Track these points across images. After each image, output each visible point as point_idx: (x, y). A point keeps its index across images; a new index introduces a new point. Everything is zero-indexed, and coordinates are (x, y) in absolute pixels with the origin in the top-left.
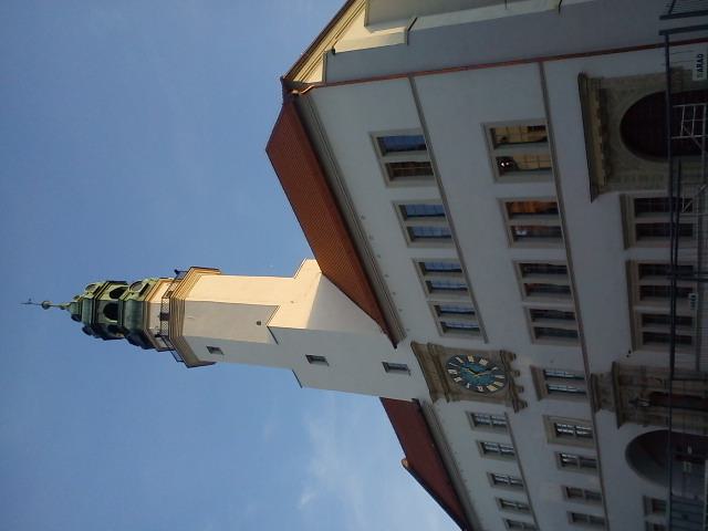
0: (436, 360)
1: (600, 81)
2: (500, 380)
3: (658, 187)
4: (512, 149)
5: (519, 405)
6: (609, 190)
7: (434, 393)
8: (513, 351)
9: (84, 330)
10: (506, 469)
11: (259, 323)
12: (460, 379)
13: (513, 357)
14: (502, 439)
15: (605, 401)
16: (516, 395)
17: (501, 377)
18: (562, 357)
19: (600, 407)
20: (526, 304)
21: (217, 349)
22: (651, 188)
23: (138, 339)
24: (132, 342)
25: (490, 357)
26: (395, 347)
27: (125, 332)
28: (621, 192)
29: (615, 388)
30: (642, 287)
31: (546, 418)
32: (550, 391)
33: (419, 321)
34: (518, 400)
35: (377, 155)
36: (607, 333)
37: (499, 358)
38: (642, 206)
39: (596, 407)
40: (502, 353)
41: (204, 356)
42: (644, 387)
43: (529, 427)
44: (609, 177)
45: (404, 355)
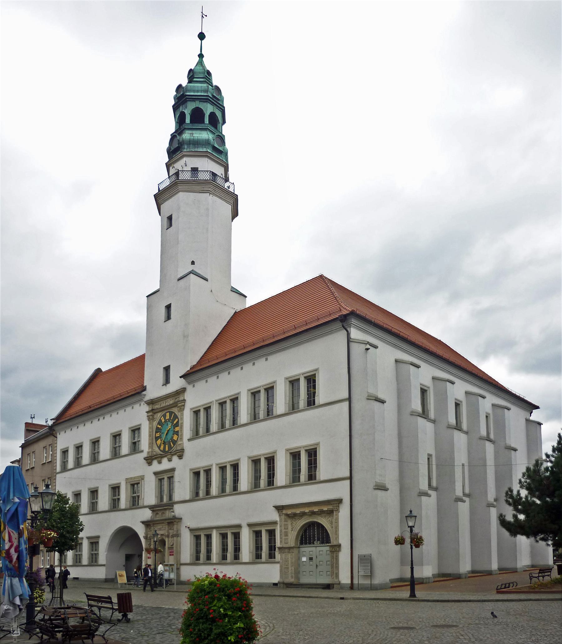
0: (175, 405)
1: (338, 510)
2: (165, 448)
3: (281, 542)
4: (306, 463)
5: (149, 460)
6: (280, 516)
7: (151, 402)
8: (184, 457)
9: (180, 86)
10: (105, 451)
11: (193, 263)
12: (163, 421)
13: (180, 457)
14: (125, 448)
15: (157, 514)
16: (156, 458)
17: (167, 449)
18: (182, 488)
19: (153, 511)
20: (214, 466)
21: (171, 225)
22: (281, 538)
23: (176, 145)
24: (173, 137)
25: (179, 443)
26: (181, 377)
27: (179, 131)
28: (279, 523)
29: (166, 520)
30: (227, 534)
31: (142, 478)
32: (161, 480)
33: (197, 396)
34: (153, 460)
35: (193, 408)
36: (194, 515)
37: (179, 448)
38: (272, 533)
39: (152, 508)
40: (182, 450)
41: (167, 206)
42: (168, 536)
43: (134, 466)
44: (287, 515)
45: (176, 383)
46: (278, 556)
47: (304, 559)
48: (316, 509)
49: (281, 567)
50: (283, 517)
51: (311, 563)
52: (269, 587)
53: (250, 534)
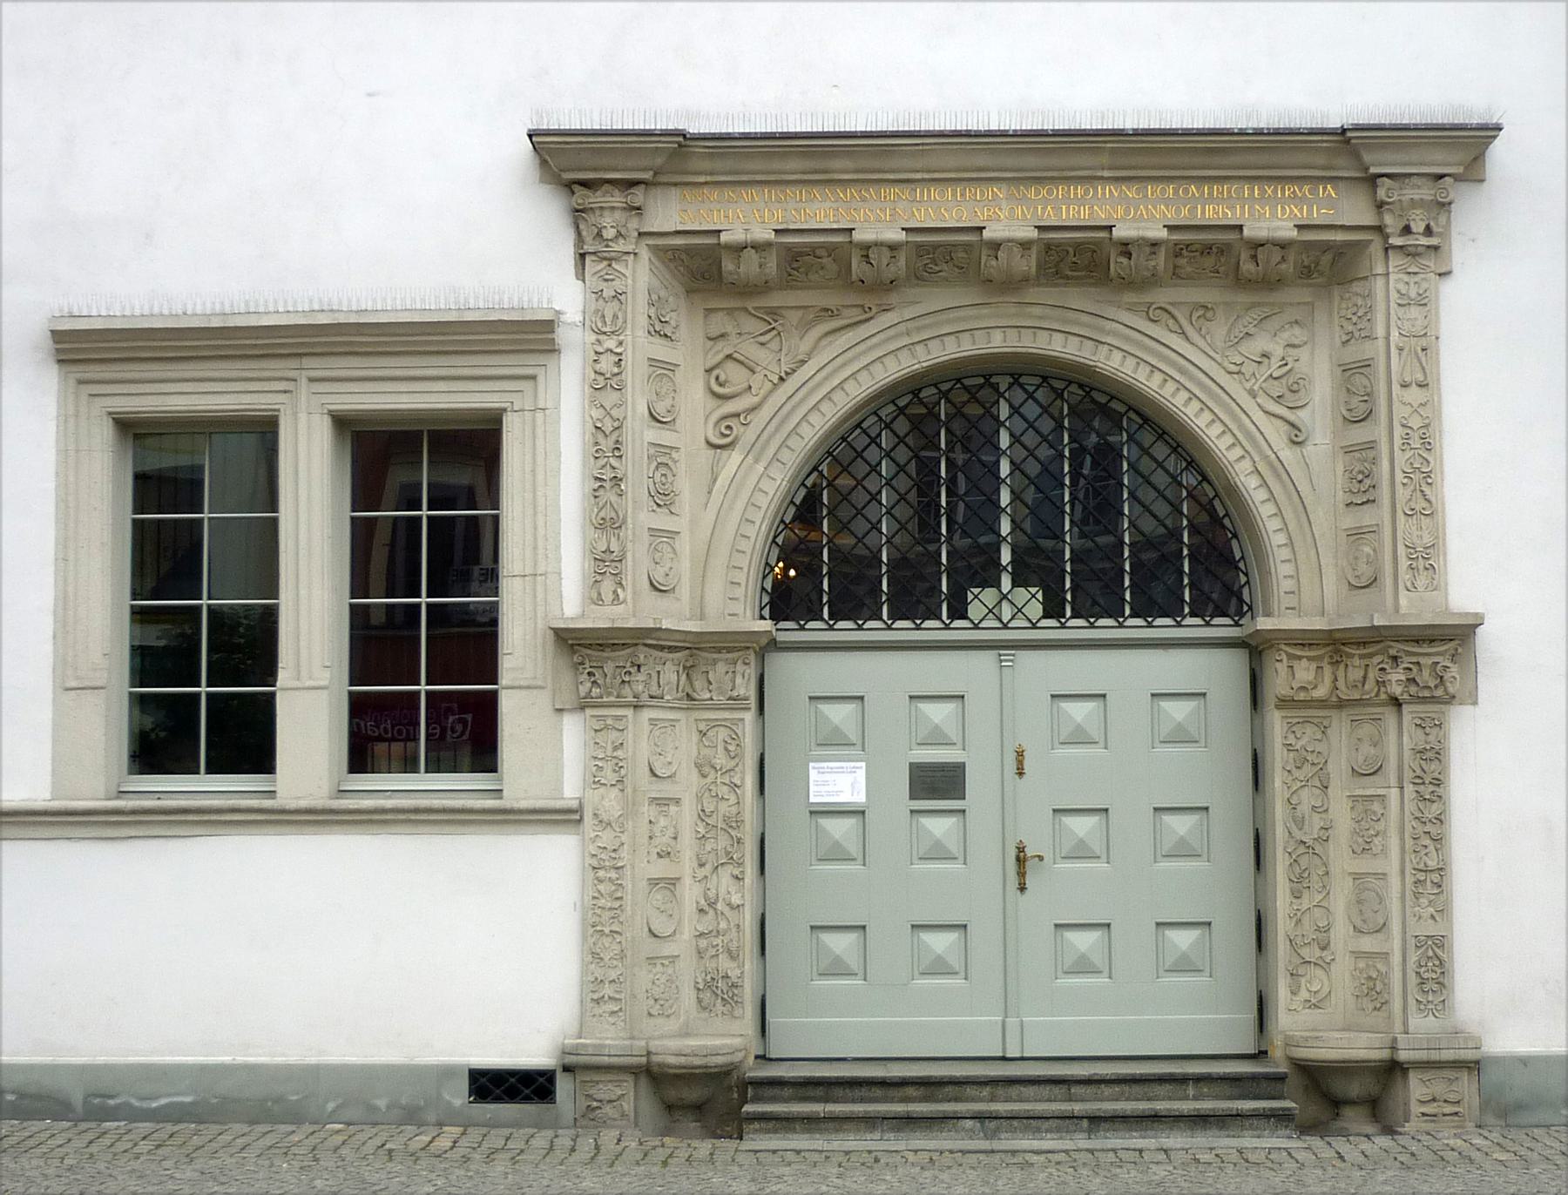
1: (1427, 250)
30: (264, 431)
46: (543, 737)
47: (838, 782)
48: (1141, 214)
49: (603, 872)
50: (639, 275)
51: (940, 827)
52: (411, 1116)
53: (70, 456)
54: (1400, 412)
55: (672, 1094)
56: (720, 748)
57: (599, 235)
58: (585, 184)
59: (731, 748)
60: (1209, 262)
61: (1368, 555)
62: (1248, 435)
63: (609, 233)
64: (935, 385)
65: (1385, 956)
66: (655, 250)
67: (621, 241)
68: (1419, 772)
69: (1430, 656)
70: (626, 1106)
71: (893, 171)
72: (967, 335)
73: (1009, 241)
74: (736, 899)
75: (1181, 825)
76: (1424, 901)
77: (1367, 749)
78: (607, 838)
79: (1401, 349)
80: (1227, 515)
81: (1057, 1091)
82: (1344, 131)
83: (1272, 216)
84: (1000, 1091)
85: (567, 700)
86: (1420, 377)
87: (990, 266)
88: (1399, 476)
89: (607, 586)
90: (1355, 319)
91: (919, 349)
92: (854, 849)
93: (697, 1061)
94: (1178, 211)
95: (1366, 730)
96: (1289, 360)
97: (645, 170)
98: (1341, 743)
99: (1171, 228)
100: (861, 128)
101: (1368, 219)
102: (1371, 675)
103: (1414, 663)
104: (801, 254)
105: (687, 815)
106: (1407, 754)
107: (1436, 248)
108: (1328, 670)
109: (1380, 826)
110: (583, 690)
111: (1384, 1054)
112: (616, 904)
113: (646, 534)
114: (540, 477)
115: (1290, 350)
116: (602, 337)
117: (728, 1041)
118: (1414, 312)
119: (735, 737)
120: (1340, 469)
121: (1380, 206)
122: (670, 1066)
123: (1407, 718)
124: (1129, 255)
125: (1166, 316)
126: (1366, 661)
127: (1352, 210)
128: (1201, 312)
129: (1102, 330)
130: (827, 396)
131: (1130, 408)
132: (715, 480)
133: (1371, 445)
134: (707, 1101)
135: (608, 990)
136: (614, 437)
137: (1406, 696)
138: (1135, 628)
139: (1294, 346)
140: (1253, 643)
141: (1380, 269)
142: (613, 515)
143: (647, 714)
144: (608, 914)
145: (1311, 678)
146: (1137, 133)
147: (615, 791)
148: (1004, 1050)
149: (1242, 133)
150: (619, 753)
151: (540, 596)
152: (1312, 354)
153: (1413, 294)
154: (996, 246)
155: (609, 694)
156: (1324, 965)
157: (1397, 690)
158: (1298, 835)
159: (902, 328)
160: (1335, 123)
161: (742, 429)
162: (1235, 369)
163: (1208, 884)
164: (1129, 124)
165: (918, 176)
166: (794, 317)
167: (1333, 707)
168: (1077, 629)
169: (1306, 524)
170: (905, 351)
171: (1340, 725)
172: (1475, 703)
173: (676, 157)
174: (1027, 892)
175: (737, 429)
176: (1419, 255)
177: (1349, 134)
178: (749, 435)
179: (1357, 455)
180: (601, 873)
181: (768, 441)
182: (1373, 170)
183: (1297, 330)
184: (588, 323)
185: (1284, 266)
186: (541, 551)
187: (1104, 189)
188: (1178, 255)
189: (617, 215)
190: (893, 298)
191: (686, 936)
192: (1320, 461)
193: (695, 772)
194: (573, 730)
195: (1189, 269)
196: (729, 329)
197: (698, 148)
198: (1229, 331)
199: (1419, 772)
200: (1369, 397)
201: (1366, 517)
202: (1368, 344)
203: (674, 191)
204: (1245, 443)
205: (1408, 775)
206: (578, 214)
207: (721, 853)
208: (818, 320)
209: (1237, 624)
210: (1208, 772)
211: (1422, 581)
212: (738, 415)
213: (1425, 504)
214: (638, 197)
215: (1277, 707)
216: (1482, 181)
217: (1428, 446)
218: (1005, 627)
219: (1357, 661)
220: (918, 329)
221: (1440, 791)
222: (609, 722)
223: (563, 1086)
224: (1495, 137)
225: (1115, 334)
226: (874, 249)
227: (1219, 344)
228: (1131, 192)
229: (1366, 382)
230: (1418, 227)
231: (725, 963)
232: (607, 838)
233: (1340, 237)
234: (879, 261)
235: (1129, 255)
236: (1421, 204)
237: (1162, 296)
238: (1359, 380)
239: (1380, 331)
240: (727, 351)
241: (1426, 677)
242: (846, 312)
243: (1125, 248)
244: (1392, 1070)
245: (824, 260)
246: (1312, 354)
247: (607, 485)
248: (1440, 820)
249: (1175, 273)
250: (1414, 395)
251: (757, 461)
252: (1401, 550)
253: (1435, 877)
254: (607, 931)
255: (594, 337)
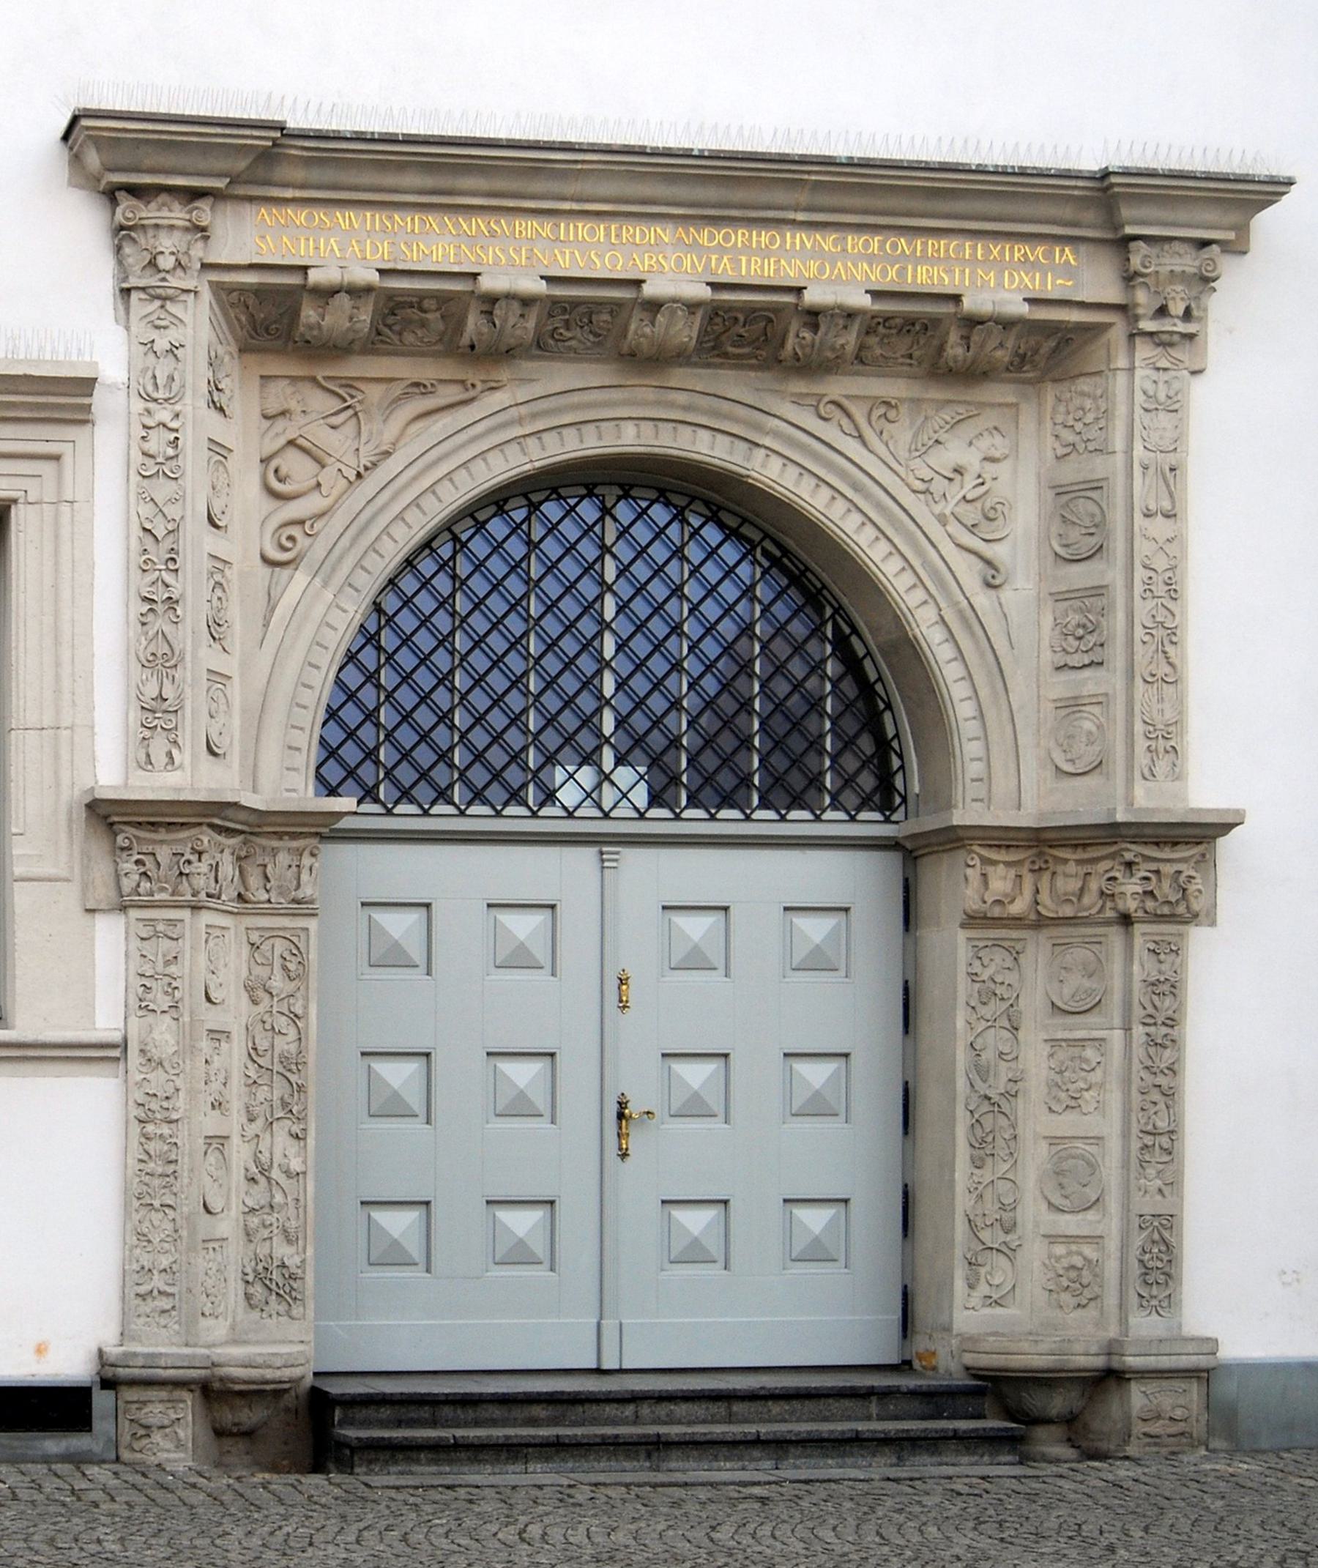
1: (1174, 334)
48: (838, 270)
50: (198, 323)
54: (1143, 548)
55: (227, 1417)
56: (277, 963)
57: (152, 264)
58: (135, 191)
59: (292, 966)
60: (902, 345)
61: (1090, 733)
62: (935, 574)
63: (166, 262)
64: (525, 496)
65: (1096, 1240)
66: (217, 288)
67: (179, 272)
68: (1150, 1010)
69: (1176, 860)
70: (181, 1434)
71: (533, 197)
72: (591, 427)
73: (674, 300)
74: (296, 1165)
75: (816, 1074)
76: (1151, 1172)
77: (1076, 981)
78: (158, 1081)
79: (1146, 468)
80: (880, 679)
81: (719, 1409)
82: (1106, 174)
83: (999, 280)
84: (645, 1410)
85: (103, 892)
86: (1166, 505)
87: (639, 330)
88: (1139, 633)
89: (159, 747)
90: (1079, 427)
91: (531, 442)
92: (540, 1100)
93: (269, 1374)
94: (884, 273)
95: (1080, 954)
96: (987, 476)
97: (219, 175)
98: (1037, 974)
99: (876, 295)
100: (503, 135)
101: (1112, 294)
102: (1094, 885)
103: (1143, 868)
104: (401, 305)
105: (235, 1053)
106: (1137, 986)
107: (1190, 337)
108: (1028, 880)
109: (1096, 1077)
110: (127, 884)
111: (1099, 1362)
112: (171, 1168)
113: (205, 676)
114: (66, 594)
115: (987, 465)
116: (151, 405)
117: (284, 1349)
118: (1164, 419)
119: (297, 951)
120: (1048, 621)
121: (1129, 278)
122: (234, 1381)
123: (1138, 941)
124: (815, 327)
125: (837, 414)
126: (1088, 868)
127: (1093, 280)
128: (882, 410)
129: (759, 428)
130: (415, 503)
131: (767, 536)
132: (273, 610)
133: (1098, 591)
134: (318, 1428)
135: (158, 1282)
136: (167, 544)
137: (1140, 914)
138: (765, 821)
139: (993, 460)
140: (909, 845)
141: (1122, 362)
142: (166, 649)
143: (206, 918)
144: (156, 1182)
145: (1008, 890)
146: (851, 163)
147: (167, 1018)
148: (599, 1359)
149: (981, 170)
150: (173, 969)
151: (65, 756)
152: (1015, 471)
153: (1162, 397)
154: (654, 306)
155: (163, 889)
156: (1009, 1252)
157: (1131, 905)
158: (982, 1088)
159: (514, 412)
160: (1091, 164)
161: (308, 541)
162: (919, 485)
163: (848, 1152)
164: (840, 150)
165: (566, 206)
166: (374, 393)
167: (1030, 927)
168: (695, 821)
169: (1002, 691)
170: (514, 447)
171: (1037, 950)
172: (1213, 923)
173: (265, 159)
174: (628, 1159)
175: (302, 542)
176: (1171, 345)
177: (1114, 180)
178: (319, 549)
179: (1077, 603)
180: (150, 1128)
181: (341, 558)
182: (1129, 230)
183: (998, 439)
184: (133, 384)
185: (999, 353)
186: (67, 696)
187: (793, 237)
188: (869, 331)
189: (177, 235)
190: (504, 374)
191: (233, 1213)
192: (1023, 610)
193: (245, 996)
194: (110, 934)
195: (878, 351)
196: (293, 405)
197: (294, 150)
198: (916, 435)
199: (1150, 1010)
200: (1099, 525)
201: (1090, 682)
202: (1099, 460)
203: (247, 209)
204: (929, 583)
205: (1138, 1012)
206: (122, 233)
207: (277, 1103)
208: (406, 396)
209: (887, 820)
210: (850, 1010)
211: (1162, 766)
212: (302, 522)
213: (1168, 669)
214: (204, 212)
215: (963, 926)
216: (1245, 253)
217: (1173, 592)
218: (606, 816)
219: (1072, 868)
220: (534, 416)
221: (1174, 1033)
222: (161, 927)
223: (102, 1401)
224: (1284, 193)
225: (776, 434)
226: (502, 303)
227: (903, 454)
228: (828, 242)
229: (1092, 508)
230: (1177, 308)
231: (282, 1251)
232: (158, 1081)
233: (1075, 316)
234: (505, 320)
235: (815, 327)
236: (1183, 277)
237: (836, 387)
238: (1083, 507)
239: (1119, 444)
240: (291, 435)
241: (1166, 889)
242: (442, 389)
243: (813, 316)
244: (1110, 1378)
245: (429, 316)
246: (1015, 471)
247: (160, 608)
248: (1173, 1070)
249: (859, 359)
250: (1159, 527)
251: (325, 584)
252: (1139, 728)
253: (1164, 1141)
254: (157, 1203)
255: (138, 405)
